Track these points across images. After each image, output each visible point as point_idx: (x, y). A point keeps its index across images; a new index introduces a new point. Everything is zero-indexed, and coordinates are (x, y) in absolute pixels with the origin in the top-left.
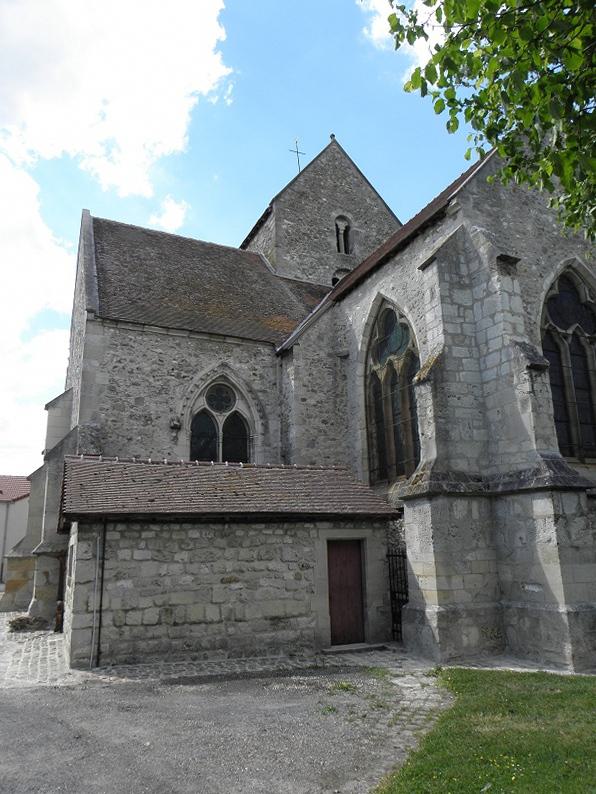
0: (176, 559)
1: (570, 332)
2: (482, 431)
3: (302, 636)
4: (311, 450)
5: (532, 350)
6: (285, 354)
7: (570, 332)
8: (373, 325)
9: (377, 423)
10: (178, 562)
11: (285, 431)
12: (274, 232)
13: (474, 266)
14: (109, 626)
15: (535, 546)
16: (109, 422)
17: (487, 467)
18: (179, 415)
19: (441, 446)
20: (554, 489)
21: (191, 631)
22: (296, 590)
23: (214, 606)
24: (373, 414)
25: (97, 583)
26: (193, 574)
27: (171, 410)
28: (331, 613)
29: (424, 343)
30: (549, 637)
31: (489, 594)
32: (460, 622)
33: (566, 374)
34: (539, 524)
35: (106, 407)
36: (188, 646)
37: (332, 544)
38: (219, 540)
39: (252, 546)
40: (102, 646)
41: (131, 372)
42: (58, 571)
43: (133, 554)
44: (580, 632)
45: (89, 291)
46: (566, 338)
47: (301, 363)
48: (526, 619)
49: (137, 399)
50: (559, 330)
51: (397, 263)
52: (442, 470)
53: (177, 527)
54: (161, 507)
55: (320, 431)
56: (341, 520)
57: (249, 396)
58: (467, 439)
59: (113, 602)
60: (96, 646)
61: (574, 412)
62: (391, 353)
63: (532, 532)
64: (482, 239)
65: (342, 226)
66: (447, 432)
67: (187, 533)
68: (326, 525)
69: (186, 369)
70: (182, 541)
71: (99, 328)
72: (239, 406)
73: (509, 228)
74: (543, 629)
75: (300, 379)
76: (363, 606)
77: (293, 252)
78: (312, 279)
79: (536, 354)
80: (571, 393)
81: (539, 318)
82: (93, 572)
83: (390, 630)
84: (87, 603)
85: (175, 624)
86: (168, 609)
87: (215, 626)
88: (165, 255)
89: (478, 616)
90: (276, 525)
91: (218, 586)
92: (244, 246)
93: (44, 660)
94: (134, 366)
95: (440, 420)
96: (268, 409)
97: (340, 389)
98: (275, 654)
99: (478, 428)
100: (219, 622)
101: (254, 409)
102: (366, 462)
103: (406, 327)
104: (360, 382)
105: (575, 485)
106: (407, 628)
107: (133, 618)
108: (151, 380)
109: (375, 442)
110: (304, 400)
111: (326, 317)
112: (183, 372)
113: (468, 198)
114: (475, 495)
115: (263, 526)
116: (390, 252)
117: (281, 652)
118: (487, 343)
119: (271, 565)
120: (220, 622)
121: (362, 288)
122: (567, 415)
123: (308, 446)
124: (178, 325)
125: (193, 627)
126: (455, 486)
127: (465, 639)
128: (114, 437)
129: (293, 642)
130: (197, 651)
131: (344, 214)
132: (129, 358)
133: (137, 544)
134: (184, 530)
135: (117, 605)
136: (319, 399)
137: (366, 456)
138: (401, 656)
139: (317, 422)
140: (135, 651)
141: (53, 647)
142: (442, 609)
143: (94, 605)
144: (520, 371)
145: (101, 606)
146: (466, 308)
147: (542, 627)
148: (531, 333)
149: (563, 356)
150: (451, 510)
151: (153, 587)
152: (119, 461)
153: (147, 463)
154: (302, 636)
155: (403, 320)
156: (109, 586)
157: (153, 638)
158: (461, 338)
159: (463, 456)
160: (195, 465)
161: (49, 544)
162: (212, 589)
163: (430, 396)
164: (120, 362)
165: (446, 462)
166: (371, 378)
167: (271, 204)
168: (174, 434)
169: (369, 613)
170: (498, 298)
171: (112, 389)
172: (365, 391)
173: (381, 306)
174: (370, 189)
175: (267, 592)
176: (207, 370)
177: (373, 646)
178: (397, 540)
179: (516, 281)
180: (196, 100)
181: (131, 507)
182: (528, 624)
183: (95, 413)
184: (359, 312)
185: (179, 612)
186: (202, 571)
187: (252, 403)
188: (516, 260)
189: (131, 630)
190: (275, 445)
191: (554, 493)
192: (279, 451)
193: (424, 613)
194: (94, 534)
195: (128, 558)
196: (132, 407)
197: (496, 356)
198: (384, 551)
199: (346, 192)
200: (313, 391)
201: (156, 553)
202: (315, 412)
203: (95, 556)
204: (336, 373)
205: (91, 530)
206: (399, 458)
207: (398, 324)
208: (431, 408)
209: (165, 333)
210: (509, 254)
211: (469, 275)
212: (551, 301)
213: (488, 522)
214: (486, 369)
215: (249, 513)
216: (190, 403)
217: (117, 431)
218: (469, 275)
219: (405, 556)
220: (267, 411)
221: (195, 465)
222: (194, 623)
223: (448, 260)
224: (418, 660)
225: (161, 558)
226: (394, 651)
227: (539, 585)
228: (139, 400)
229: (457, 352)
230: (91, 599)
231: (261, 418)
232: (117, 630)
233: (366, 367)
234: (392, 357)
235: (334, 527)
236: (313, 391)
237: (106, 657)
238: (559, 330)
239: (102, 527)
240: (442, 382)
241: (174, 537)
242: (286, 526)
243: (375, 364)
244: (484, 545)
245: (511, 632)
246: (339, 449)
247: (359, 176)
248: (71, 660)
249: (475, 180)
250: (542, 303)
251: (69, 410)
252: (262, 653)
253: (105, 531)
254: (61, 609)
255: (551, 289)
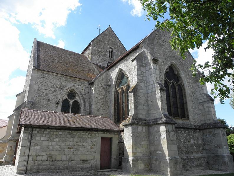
0: (54, 140)
1: (172, 82)
2: (147, 107)
3: (92, 166)
4: (98, 112)
5: (161, 85)
6: (92, 84)
7: (172, 82)
8: (118, 77)
9: (118, 105)
10: (55, 141)
11: (90, 106)
12: (91, 50)
13: (146, 61)
14: (31, 161)
15: (160, 139)
16: (37, 100)
17: (148, 117)
18: (59, 100)
19: (135, 110)
20: (166, 124)
21: (57, 163)
22: (91, 152)
23: (65, 156)
24: (117, 102)
25: (28, 147)
26: (59, 145)
27: (56, 98)
28: (101, 160)
29: (132, 82)
30: (163, 167)
31: (147, 154)
32: (138, 162)
33: (170, 93)
34: (162, 133)
35: (36, 96)
36: (56, 168)
37: (102, 138)
38: (68, 135)
39: (78, 138)
40: (28, 167)
41: (45, 86)
42: (15, 146)
43: (41, 138)
44: (172, 164)
45: (34, 60)
46: (170, 83)
47: (96, 87)
48: (157, 161)
49: (46, 94)
50: (169, 81)
51: (125, 60)
52: (135, 118)
53: (55, 131)
54: (50, 124)
55: (101, 107)
56: (106, 131)
57: (80, 96)
58: (143, 109)
59: (33, 153)
60: (26, 167)
61: (172, 104)
62: (122, 85)
63: (160, 136)
64: (149, 54)
65: (111, 50)
66: (137, 106)
67: (58, 133)
68: (101, 132)
69: (62, 86)
70: (56, 135)
71: (36, 72)
72: (77, 98)
73: (156, 52)
74: (162, 164)
75: (96, 91)
76: (110, 158)
77: (96, 56)
78: (101, 64)
79: (162, 86)
80: (171, 98)
81: (163, 77)
82: (27, 143)
83: (118, 165)
84: (24, 153)
85: (52, 161)
86: (50, 156)
87: (65, 162)
88: (58, 53)
89: (144, 160)
90: (86, 132)
91: (67, 149)
92: (83, 53)
93: (7, 172)
94: (46, 84)
95: (135, 103)
96: (86, 100)
97: (107, 95)
98: (83, 171)
99: (146, 106)
100: (66, 161)
101: (81, 100)
102: (114, 117)
103: (127, 78)
104: (113, 93)
105: (172, 122)
106: (123, 164)
107: (39, 158)
108: (51, 89)
109: (117, 111)
110: (97, 97)
111: (105, 74)
112: (61, 87)
113: (145, 43)
114: (145, 125)
115: (82, 132)
116: (123, 57)
117: (85, 171)
118: (149, 82)
119: (84, 144)
120: (67, 161)
121: (115, 66)
122: (170, 104)
123: (97, 111)
124: (60, 73)
125: (58, 162)
126: (139, 122)
127: (140, 167)
128: (38, 105)
129: (89, 168)
130: (58, 170)
131: (112, 47)
132: (45, 81)
133: (43, 135)
134: (58, 132)
135: (34, 154)
136: (101, 97)
137: (114, 115)
138: (121, 173)
139: (100, 104)
140: (39, 169)
141: (11, 169)
142: (133, 158)
143: (27, 154)
144: (158, 90)
145: (29, 154)
146: (144, 72)
147: (161, 163)
148: (161, 81)
149: (169, 88)
150: (137, 129)
151: (46, 149)
152: (39, 111)
153: (48, 112)
154: (92, 166)
155: (126, 76)
156: (32, 148)
157: (45, 165)
158: (142, 80)
159: (141, 114)
160: (63, 113)
161: (13, 137)
162: (65, 150)
163: (133, 96)
164: (42, 82)
165: (137, 115)
166: (116, 92)
167: (91, 42)
168: (57, 105)
169: (112, 160)
170: (152, 70)
171: (38, 90)
172: (115, 96)
173: (120, 72)
174: (119, 41)
175: (82, 152)
176: (68, 87)
177: (113, 170)
178: (121, 140)
179: (157, 66)
180: (70, 11)
181: (41, 123)
182: (158, 163)
183: (32, 97)
184: (114, 74)
185: (54, 157)
186: (62, 144)
187: (81, 98)
188: (158, 60)
189: (38, 162)
190: (87, 111)
191: (166, 124)
192: (88, 112)
193: (128, 159)
194: (29, 131)
195: (39, 139)
196: (44, 96)
197: (151, 86)
198: (118, 141)
199: (112, 41)
200: (99, 95)
201: (48, 138)
202: (99, 101)
203: (28, 138)
204: (106, 90)
205: (28, 130)
206: (123, 115)
207: (125, 77)
208: (133, 99)
209: (56, 75)
210: (156, 58)
211: (145, 64)
212: (167, 73)
213: (148, 133)
214: (149, 85)
215: (78, 127)
216: (62, 96)
217: (39, 103)
218: (145, 64)
219: (123, 143)
220: (85, 100)
221: (63, 113)
222: (58, 161)
223: (140, 60)
224: (126, 173)
225: (50, 140)
226: (119, 171)
227: (161, 151)
228: (47, 94)
229: (141, 84)
230: (26, 152)
231: (84, 102)
232: (33, 162)
233: (115, 89)
234: (123, 86)
235: (103, 133)
236: (99, 95)
237: (29, 171)
238: (169, 81)
239: (32, 129)
240: (136, 92)
241: (54, 133)
242: (89, 132)
243: (118, 88)
244: (146, 140)
245: (153, 165)
246: (106, 113)
247: (116, 37)
248: (17, 171)
249: (147, 39)
250: (164, 73)
251: (24, 97)
252: (79, 171)
253: (33, 130)
254: (15, 158)
255: (167, 70)
